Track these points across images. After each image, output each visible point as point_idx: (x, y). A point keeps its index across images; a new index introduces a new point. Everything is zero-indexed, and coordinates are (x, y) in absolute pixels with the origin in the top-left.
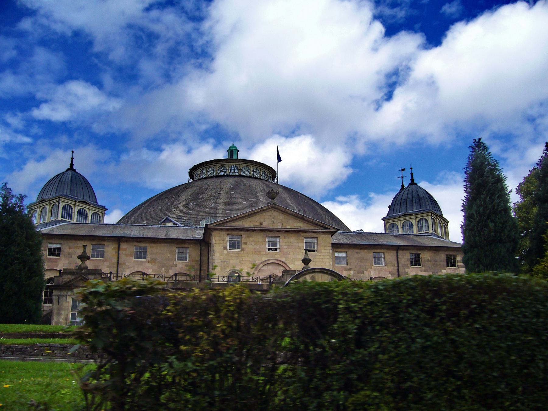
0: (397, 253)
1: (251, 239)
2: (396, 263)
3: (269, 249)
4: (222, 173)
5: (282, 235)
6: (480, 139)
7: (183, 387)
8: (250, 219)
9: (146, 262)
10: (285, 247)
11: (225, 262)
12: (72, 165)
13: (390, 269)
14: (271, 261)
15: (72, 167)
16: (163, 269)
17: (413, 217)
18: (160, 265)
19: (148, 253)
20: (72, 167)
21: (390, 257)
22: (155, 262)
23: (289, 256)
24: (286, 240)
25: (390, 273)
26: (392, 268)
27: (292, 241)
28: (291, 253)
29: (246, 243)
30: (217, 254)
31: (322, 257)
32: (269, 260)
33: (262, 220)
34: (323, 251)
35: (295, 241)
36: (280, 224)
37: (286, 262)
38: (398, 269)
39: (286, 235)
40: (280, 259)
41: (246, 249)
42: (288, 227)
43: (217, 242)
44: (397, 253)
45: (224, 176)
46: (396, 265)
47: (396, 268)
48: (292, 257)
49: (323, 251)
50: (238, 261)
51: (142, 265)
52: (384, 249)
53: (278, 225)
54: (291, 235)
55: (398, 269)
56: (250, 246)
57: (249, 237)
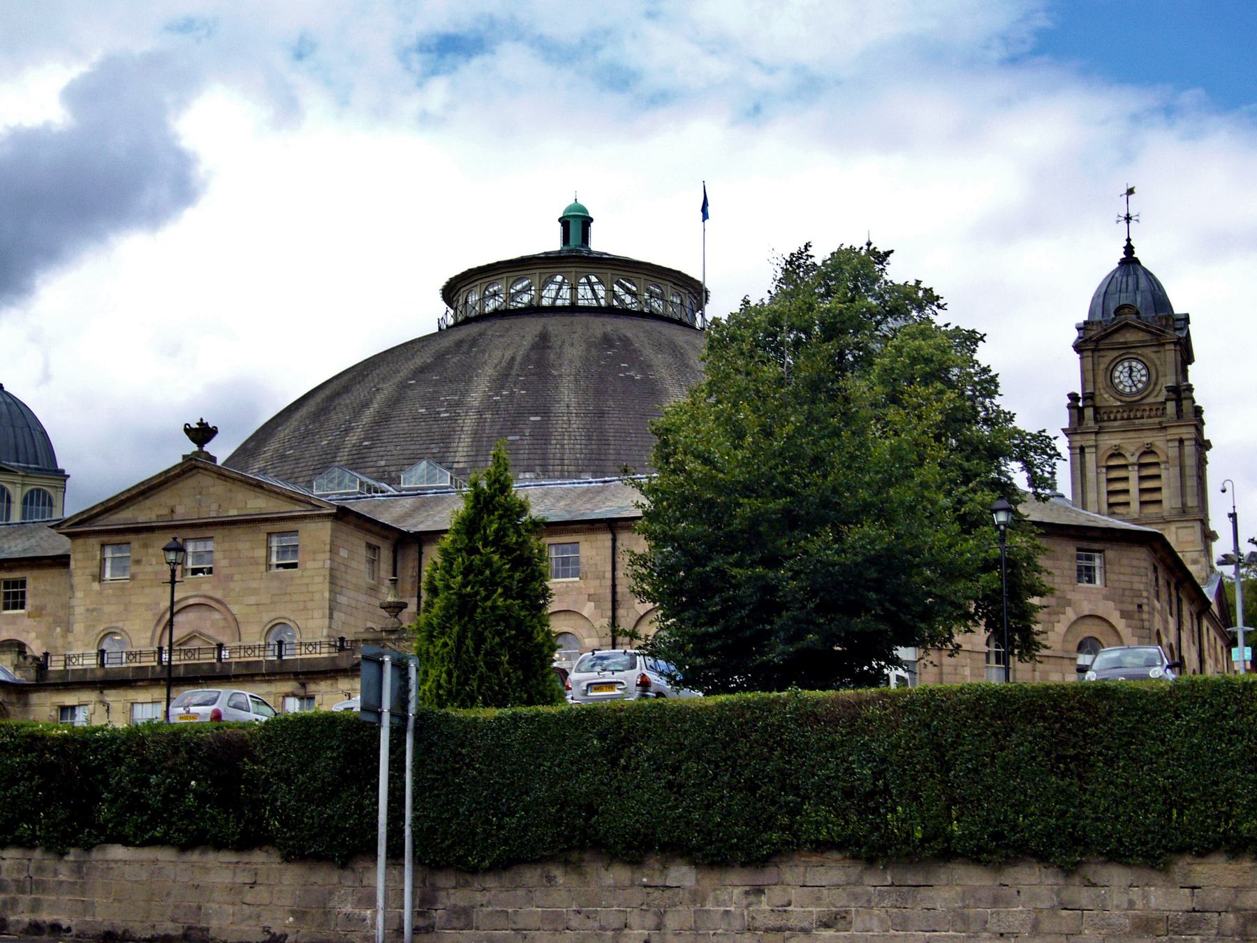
0: (614, 541)
1: (150, 551)
2: (609, 568)
3: (195, 571)
4: (491, 305)
5: (218, 533)
6: (576, 223)
7: (289, 785)
8: (148, 503)
9: (22, 615)
10: (224, 563)
11: (93, 610)
12: (1129, 249)
13: (592, 586)
14: (191, 601)
15: (1129, 260)
16: (58, 629)
17: (18, 479)
18: (51, 619)
19: (27, 595)
20: (1129, 260)
21: (594, 552)
22: (40, 615)
23: (232, 585)
24: (226, 546)
25: (590, 598)
26: (597, 582)
27: (240, 546)
28: (236, 577)
29: (138, 562)
30: (79, 594)
31: (306, 581)
32: (186, 598)
33: (172, 502)
34: (310, 565)
35: (248, 545)
36: (214, 507)
37: (226, 600)
38: (614, 586)
39: (226, 532)
40: (211, 594)
41: (140, 577)
42: (233, 512)
43: (80, 564)
44: (614, 541)
45: (497, 314)
46: (609, 575)
47: (609, 582)
48: (236, 586)
49: (310, 565)
50: (122, 607)
51: (15, 623)
52: (576, 532)
53: (211, 511)
54: (237, 531)
55: (614, 586)
56: (149, 569)
57: (145, 546)
